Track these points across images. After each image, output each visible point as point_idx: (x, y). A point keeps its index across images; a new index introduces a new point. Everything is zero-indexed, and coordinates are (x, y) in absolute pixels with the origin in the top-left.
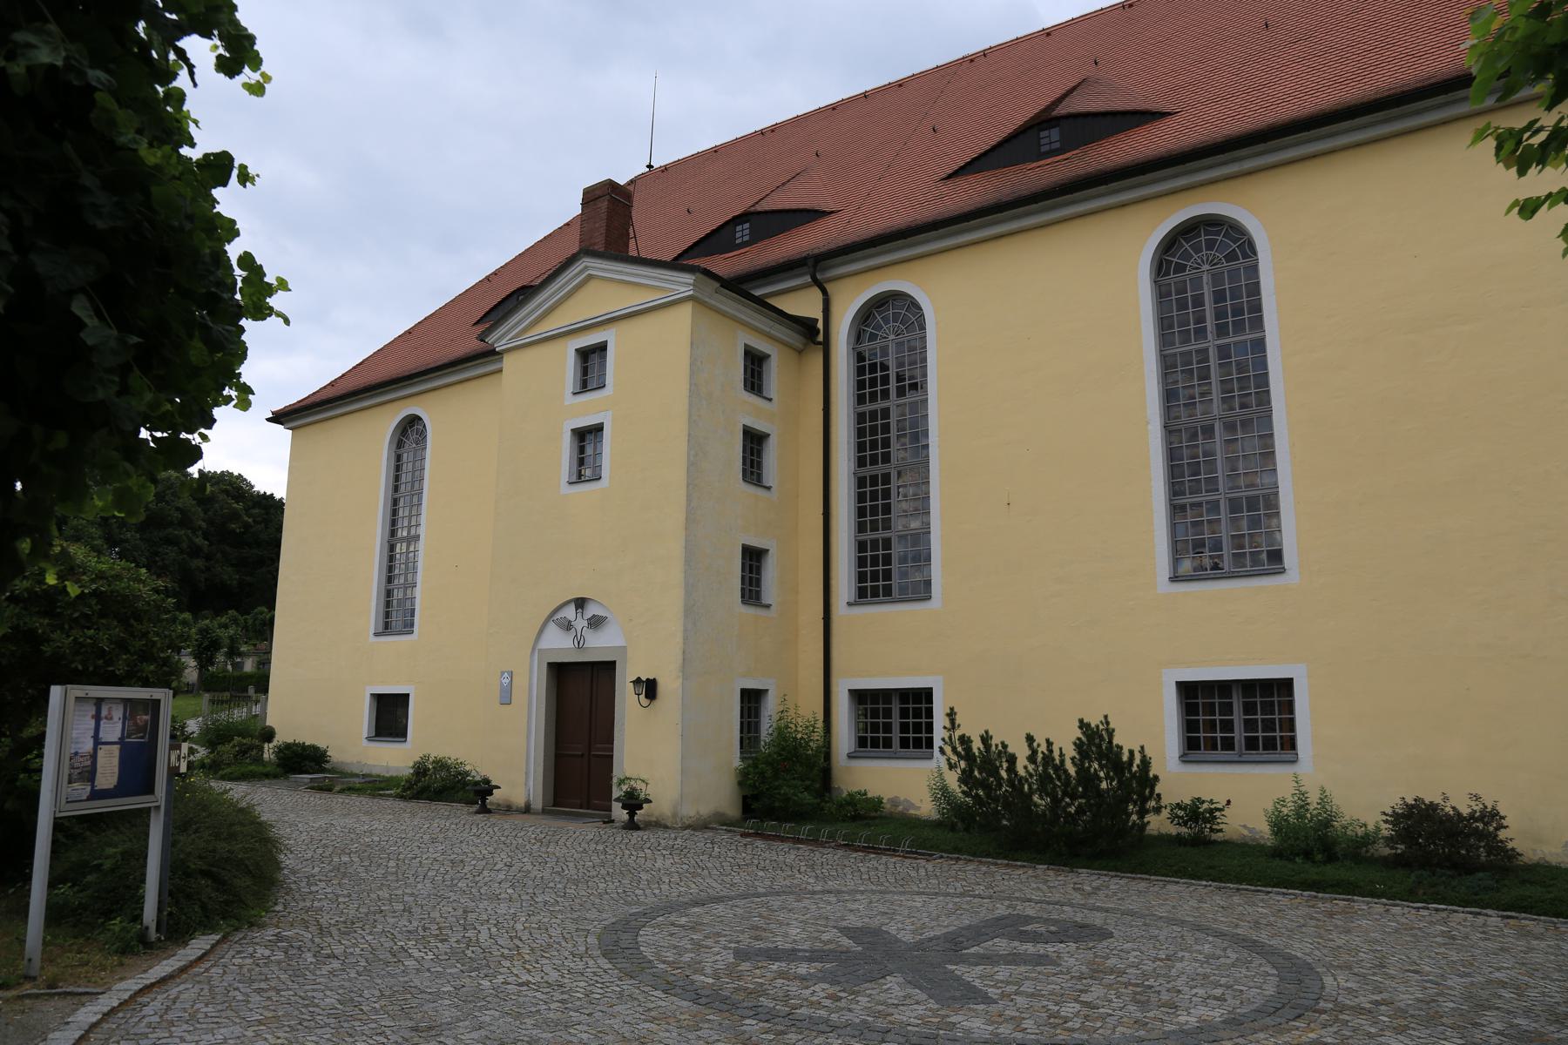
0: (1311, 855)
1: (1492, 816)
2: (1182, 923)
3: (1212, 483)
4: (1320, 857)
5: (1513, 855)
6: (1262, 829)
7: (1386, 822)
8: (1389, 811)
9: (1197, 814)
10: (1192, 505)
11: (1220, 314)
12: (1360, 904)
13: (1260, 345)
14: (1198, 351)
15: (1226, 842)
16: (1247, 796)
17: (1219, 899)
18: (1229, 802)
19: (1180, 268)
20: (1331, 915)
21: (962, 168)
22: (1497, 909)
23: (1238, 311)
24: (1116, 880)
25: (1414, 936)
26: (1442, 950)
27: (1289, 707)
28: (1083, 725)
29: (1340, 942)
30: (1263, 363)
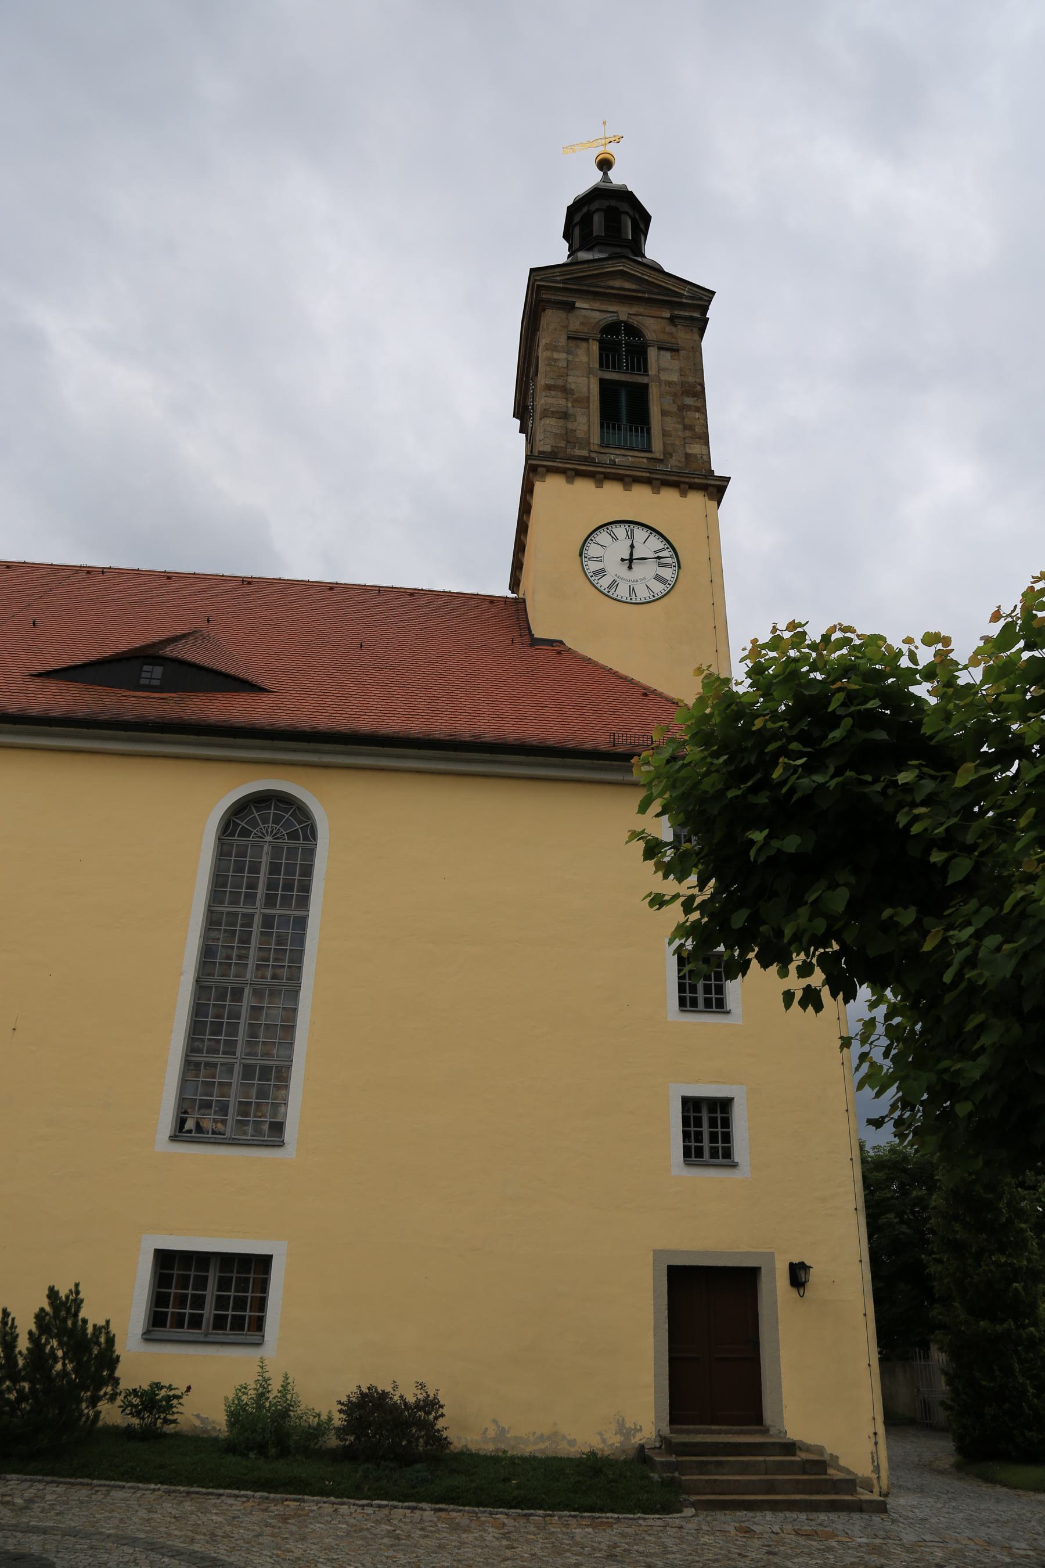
0: (267, 1450)
1: (431, 1404)
2: (133, 1542)
3: (230, 1048)
4: (274, 1450)
5: (442, 1443)
6: (218, 1419)
7: (341, 1411)
8: (344, 1399)
9: (154, 1402)
10: (207, 1064)
11: (272, 885)
12: (311, 1504)
13: (301, 923)
14: (244, 915)
15: (177, 1435)
16: (206, 1381)
17: (169, 1507)
18: (189, 1388)
19: (245, 833)
20: (284, 1519)
21: (56, 671)
22: (432, 1502)
23: (288, 886)
24: (50, 1488)
25: (364, 1538)
26: (391, 1553)
27: (263, 1285)
28: (52, 1294)
29: (298, 1553)
30: (301, 940)
